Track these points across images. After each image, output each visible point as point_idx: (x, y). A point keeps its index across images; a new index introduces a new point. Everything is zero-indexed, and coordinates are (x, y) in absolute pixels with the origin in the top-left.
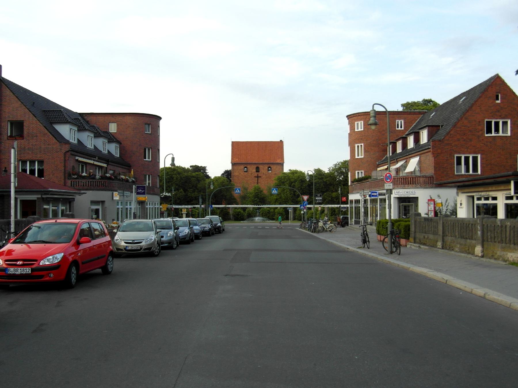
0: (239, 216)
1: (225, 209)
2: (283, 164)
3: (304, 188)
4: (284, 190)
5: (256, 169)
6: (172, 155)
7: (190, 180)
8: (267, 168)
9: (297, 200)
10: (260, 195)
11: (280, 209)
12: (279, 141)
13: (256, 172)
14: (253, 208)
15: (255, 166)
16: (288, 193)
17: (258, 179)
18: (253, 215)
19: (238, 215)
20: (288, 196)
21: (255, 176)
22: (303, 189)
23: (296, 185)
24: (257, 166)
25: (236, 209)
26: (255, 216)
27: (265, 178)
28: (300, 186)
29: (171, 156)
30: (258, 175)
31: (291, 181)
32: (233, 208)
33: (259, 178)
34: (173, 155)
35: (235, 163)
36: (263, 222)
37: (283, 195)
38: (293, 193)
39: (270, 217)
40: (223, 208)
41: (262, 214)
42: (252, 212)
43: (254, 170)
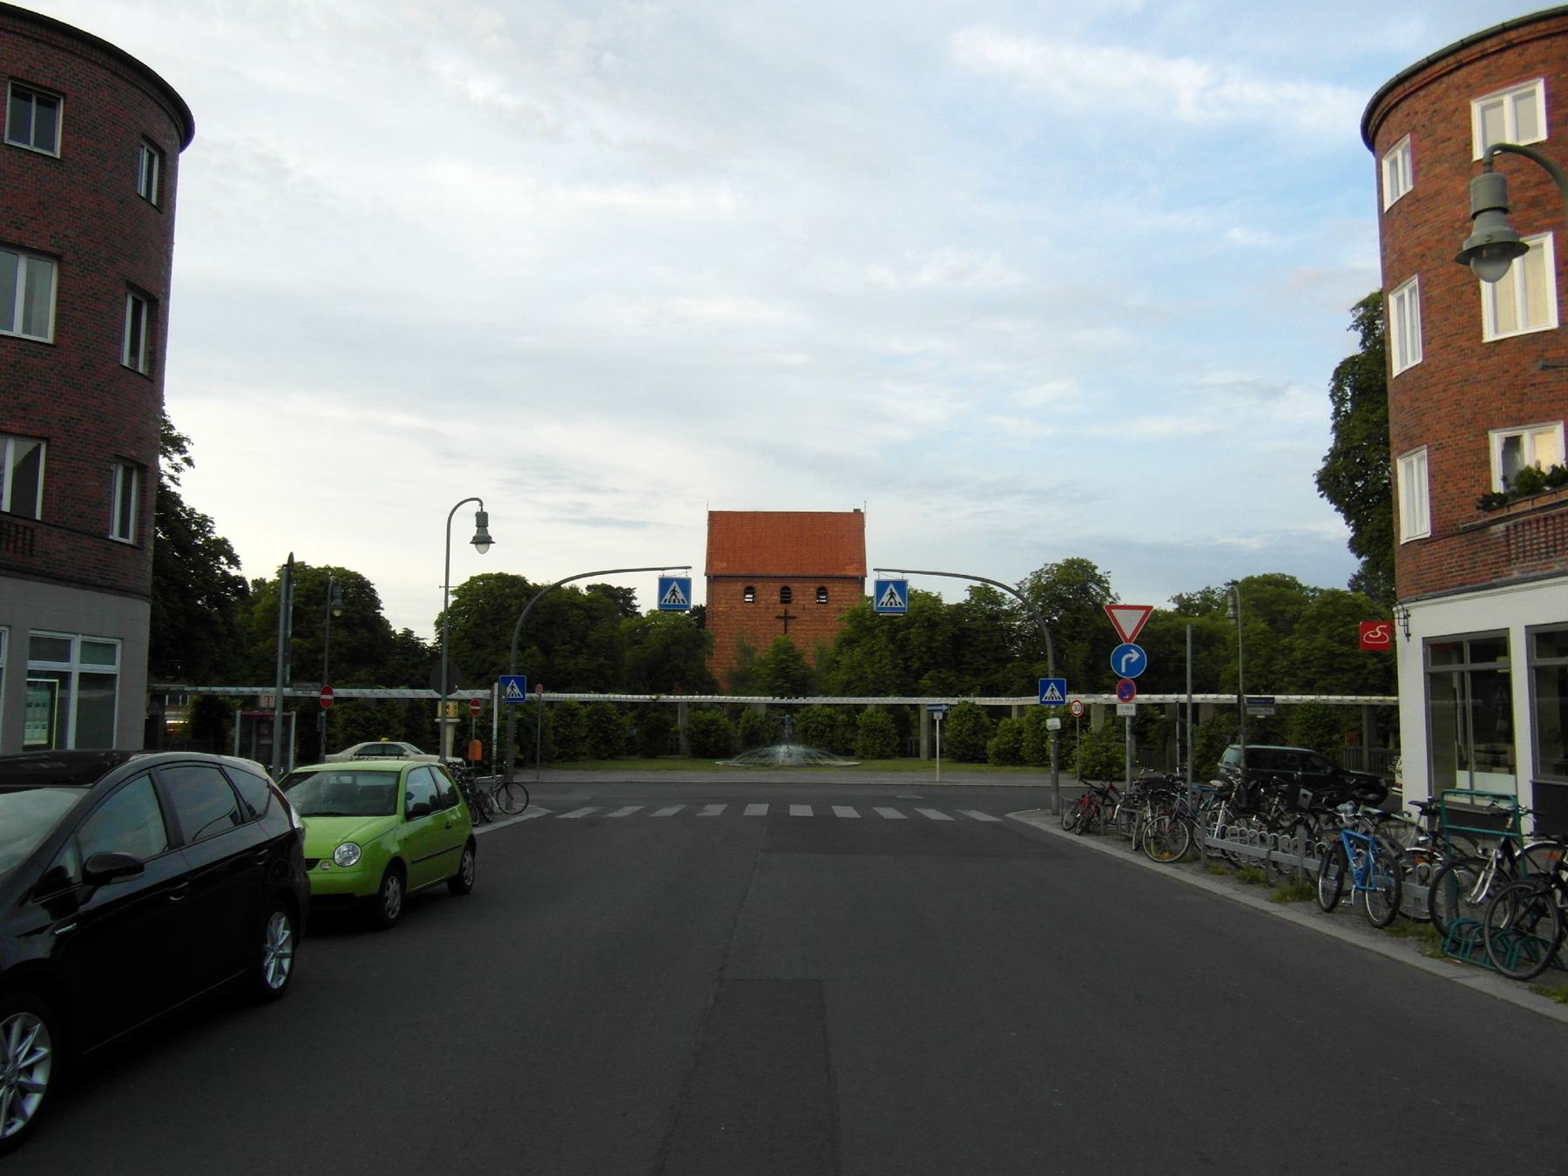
0: (712, 739)
1: (655, 710)
2: (863, 579)
3: (937, 647)
4: (873, 653)
5: (781, 593)
6: (478, 503)
7: (566, 617)
8: (813, 591)
9: (914, 686)
10: (795, 669)
11: (877, 712)
12: (852, 511)
13: (782, 602)
14: (771, 706)
15: (779, 584)
16: (885, 662)
17: (786, 626)
18: (766, 735)
19: (706, 733)
20: (887, 672)
21: (776, 615)
22: (934, 650)
23: (911, 636)
24: (784, 584)
25: (700, 709)
26: (777, 740)
27: (806, 621)
28: (925, 639)
29: (474, 507)
30: (786, 612)
31: (895, 623)
32: (689, 704)
33: (791, 622)
34: (481, 504)
35: (718, 573)
36: (809, 765)
37: (869, 670)
38: (901, 661)
39: (834, 744)
40: (646, 704)
41: (806, 730)
42: (761, 723)
43: (775, 598)
